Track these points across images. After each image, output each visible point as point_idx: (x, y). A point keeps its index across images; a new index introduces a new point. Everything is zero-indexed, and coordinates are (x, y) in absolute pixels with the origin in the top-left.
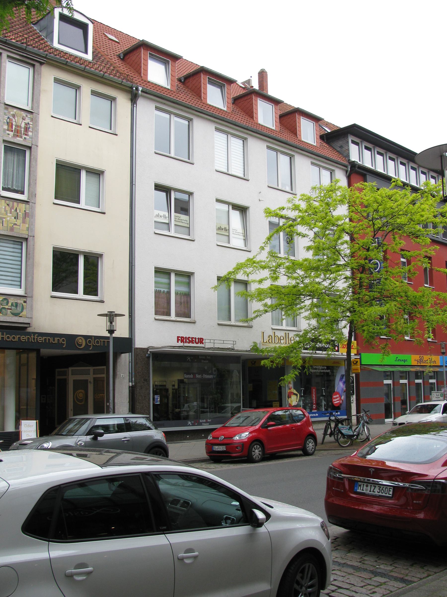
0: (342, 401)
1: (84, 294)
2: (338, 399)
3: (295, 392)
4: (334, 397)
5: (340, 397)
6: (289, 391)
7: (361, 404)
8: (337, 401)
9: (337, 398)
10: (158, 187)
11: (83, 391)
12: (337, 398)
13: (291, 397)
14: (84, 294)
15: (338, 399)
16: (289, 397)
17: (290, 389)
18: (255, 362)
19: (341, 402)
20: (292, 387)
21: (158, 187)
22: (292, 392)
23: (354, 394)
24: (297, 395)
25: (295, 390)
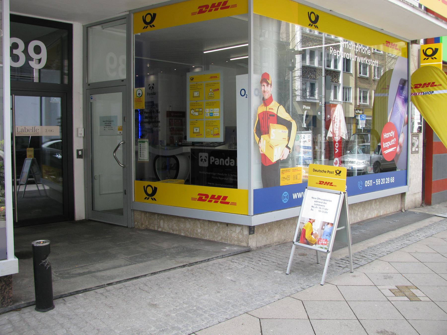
0: (401, 147)
1: (254, 190)
2: (393, 141)
3: (283, 114)
4: (386, 136)
5: (397, 136)
6: (262, 109)
7: (434, 156)
8: (390, 147)
9: (389, 139)
10: (144, 28)
11: (201, 164)
12: (389, 139)
13: (267, 132)
14: (254, 190)
15: (393, 141)
16: (262, 130)
17: (266, 102)
18: (154, 17)
19: (398, 150)
20: (274, 97)
21: (144, 28)
22: (273, 115)
23: (421, 132)
24: (288, 125)
25: (282, 109)
